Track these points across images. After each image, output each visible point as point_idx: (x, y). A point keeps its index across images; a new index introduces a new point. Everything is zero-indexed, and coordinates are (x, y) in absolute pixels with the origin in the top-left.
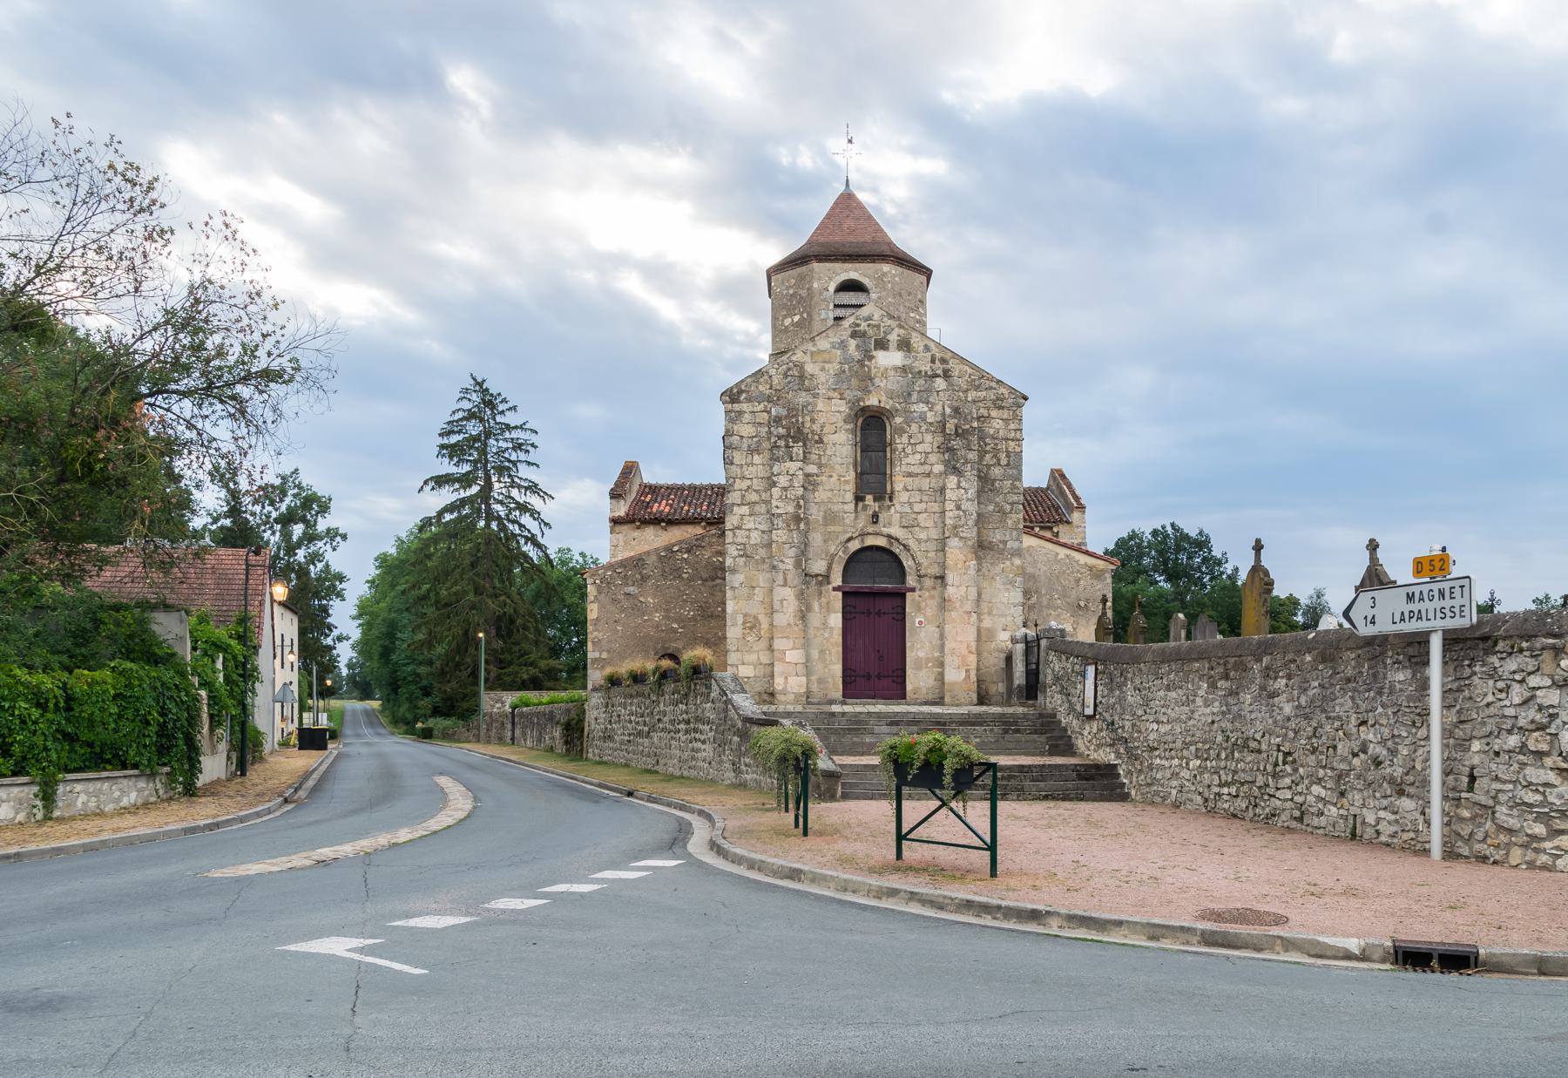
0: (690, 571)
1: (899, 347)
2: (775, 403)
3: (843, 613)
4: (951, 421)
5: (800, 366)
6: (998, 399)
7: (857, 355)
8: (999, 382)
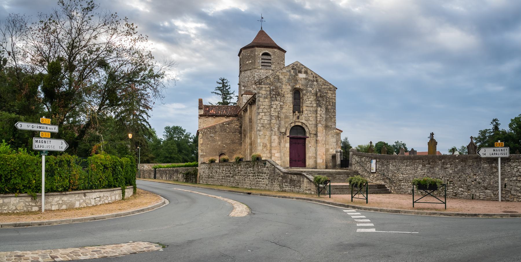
1: (305, 73)
2: (271, 86)
3: (290, 143)
5: (278, 76)
7: (293, 74)
8: (330, 84)
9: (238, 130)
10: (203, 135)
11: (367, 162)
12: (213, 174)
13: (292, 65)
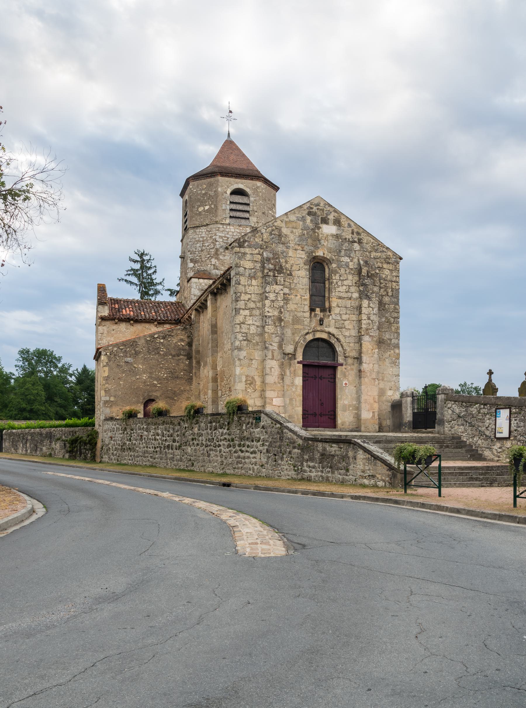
0: (165, 350)
1: (335, 224)
3: (303, 377)
4: (365, 268)
5: (279, 229)
6: (387, 258)
7: (311, 226)
8: (387, 248)
9: (183, 350)
10: (109, 359)
11: (485, 414)
12: (134, 442)
13: (308, 205)
